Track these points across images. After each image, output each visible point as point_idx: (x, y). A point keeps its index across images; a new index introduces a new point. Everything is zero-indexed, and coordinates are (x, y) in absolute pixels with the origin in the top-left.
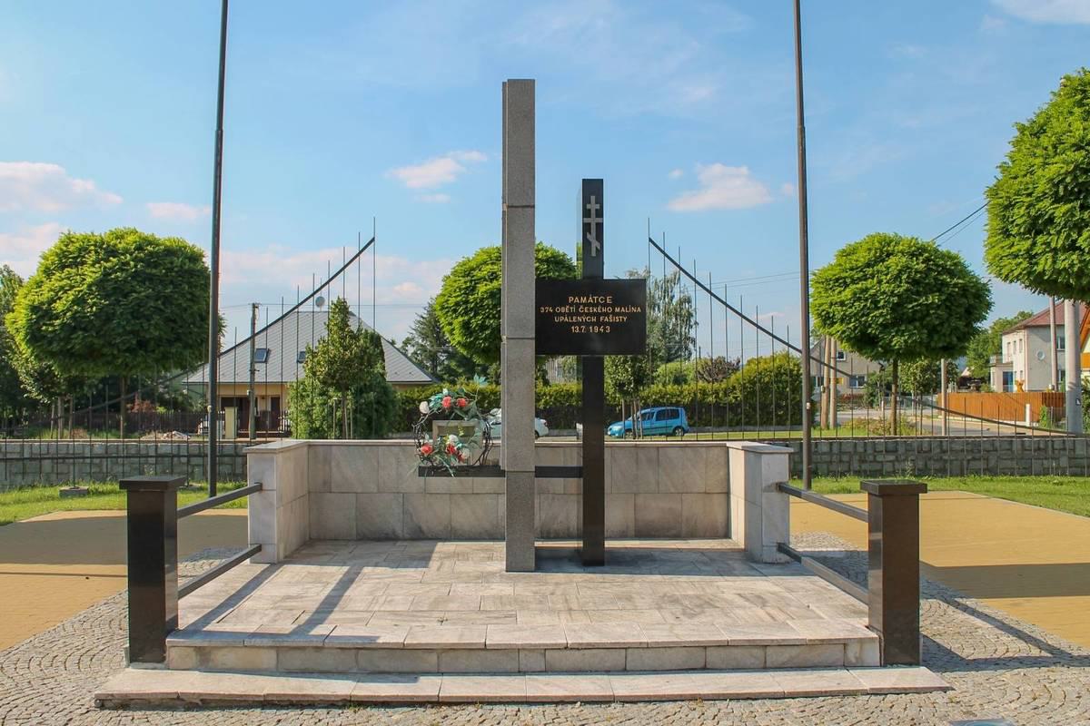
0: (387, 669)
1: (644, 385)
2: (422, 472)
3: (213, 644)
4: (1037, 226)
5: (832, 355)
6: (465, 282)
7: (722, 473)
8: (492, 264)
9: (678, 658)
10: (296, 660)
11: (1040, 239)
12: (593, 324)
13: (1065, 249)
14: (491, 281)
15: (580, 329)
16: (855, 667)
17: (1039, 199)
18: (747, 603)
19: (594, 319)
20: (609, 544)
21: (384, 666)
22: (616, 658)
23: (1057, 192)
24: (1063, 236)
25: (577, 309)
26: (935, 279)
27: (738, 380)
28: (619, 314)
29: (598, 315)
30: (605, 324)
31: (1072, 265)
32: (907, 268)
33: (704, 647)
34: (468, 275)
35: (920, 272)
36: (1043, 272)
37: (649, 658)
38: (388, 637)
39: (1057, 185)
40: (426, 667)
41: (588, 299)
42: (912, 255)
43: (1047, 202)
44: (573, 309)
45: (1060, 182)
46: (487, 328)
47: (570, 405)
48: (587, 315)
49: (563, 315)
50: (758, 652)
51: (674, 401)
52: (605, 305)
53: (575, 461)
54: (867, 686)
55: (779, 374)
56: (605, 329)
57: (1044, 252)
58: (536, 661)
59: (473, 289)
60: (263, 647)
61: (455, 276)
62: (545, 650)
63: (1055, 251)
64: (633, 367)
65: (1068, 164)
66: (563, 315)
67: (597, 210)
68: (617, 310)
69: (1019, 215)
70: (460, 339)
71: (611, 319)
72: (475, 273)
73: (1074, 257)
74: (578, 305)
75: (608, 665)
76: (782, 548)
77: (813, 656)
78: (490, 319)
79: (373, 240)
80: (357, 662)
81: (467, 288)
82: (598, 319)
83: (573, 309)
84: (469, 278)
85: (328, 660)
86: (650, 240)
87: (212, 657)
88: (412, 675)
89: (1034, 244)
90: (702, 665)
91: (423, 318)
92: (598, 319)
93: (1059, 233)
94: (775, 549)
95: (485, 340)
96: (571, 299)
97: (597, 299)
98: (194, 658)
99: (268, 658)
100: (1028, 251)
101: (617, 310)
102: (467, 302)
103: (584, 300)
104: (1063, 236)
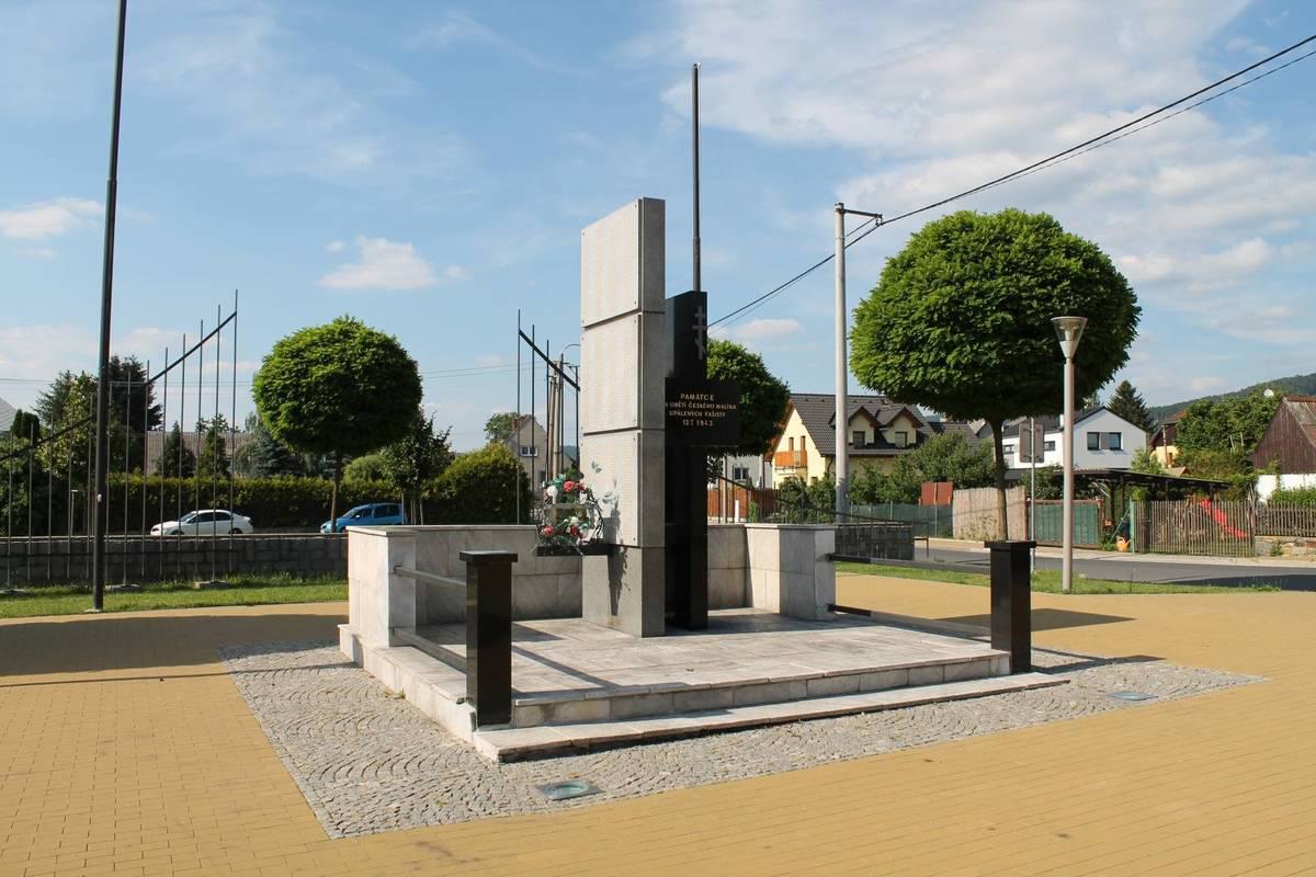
0: (695, 707)
1: (427, 477)
2: (541, 552)
3: (559, 700)
4: (910, 345)
5: (555, 450)
6: (296, 364)
7: (741, 550)
8: (324, 346)
9: (892, 678)
10: (627, 707)
11: (914, 355)
13: (933, 365)
14: (326, 364)
16: (996, 676)
17: (914, 322)
18: (811, 650)
20: (711, 613)
21: (693, 704)
22: (852, 682)
23: (932, 318)
24: (933, 354)
26: (748, 379)
27: (453, 475)
29: (688, 409)
30: (708, 418)
31: (940, 377)
32: (724, 369)
33: (908, 669)
34: (296, 357)
35: (736, 374)
36: (913, 382)
37: (874, 680)
38: (693, 680)
39: (932, 313)
40: (725, 702)
42: (727, 357)
43: (923, 326)
44: (684, 405)
45: (936, 310)
46: (320, 414)
47: (271, 501)
48: (695, 410)
49: (677, 409)
50: (939, 670)
51: (386, 496)
52: (709, 402)
54: (1025, 684)
55: (495, 469)
57: (917, 367)
58: (800, 690)
59: (304, 373)
60: (598, 699)
61: (280, 356)
62: (807, 680)
63: (926, 366)
64: (417, 458)
65: (944, 296)
66: (677, 409)
68: (718, 406)
69: (897, 336)
70: (286, 425)
71: (713, 414)
72: (305, 355)
73: (943, 370)
74: (688, 401)
75: (848, 688)
76: (832, 608)
77: (973, 670)
78: (325, 405)
79: (235, 314)
80: (673, 704)
81: (299, 371)
83: (684, 405)
84: (297, 360)
85: (650, 705)
86: (521, 333)
87: (557, 712)
88: (722, 709)
89: (907, 359)
90: (941, 680)
91: (49, 397)
93: (931, 350)
94: (826, 609)
95: (316, 427)
96: (682, 396)
98: (538, 715)
99: (603, 708)
100: (900, 364)
101: (718, 406)
102: (298, 385)
103: (692, 397)
104: (933, 354)
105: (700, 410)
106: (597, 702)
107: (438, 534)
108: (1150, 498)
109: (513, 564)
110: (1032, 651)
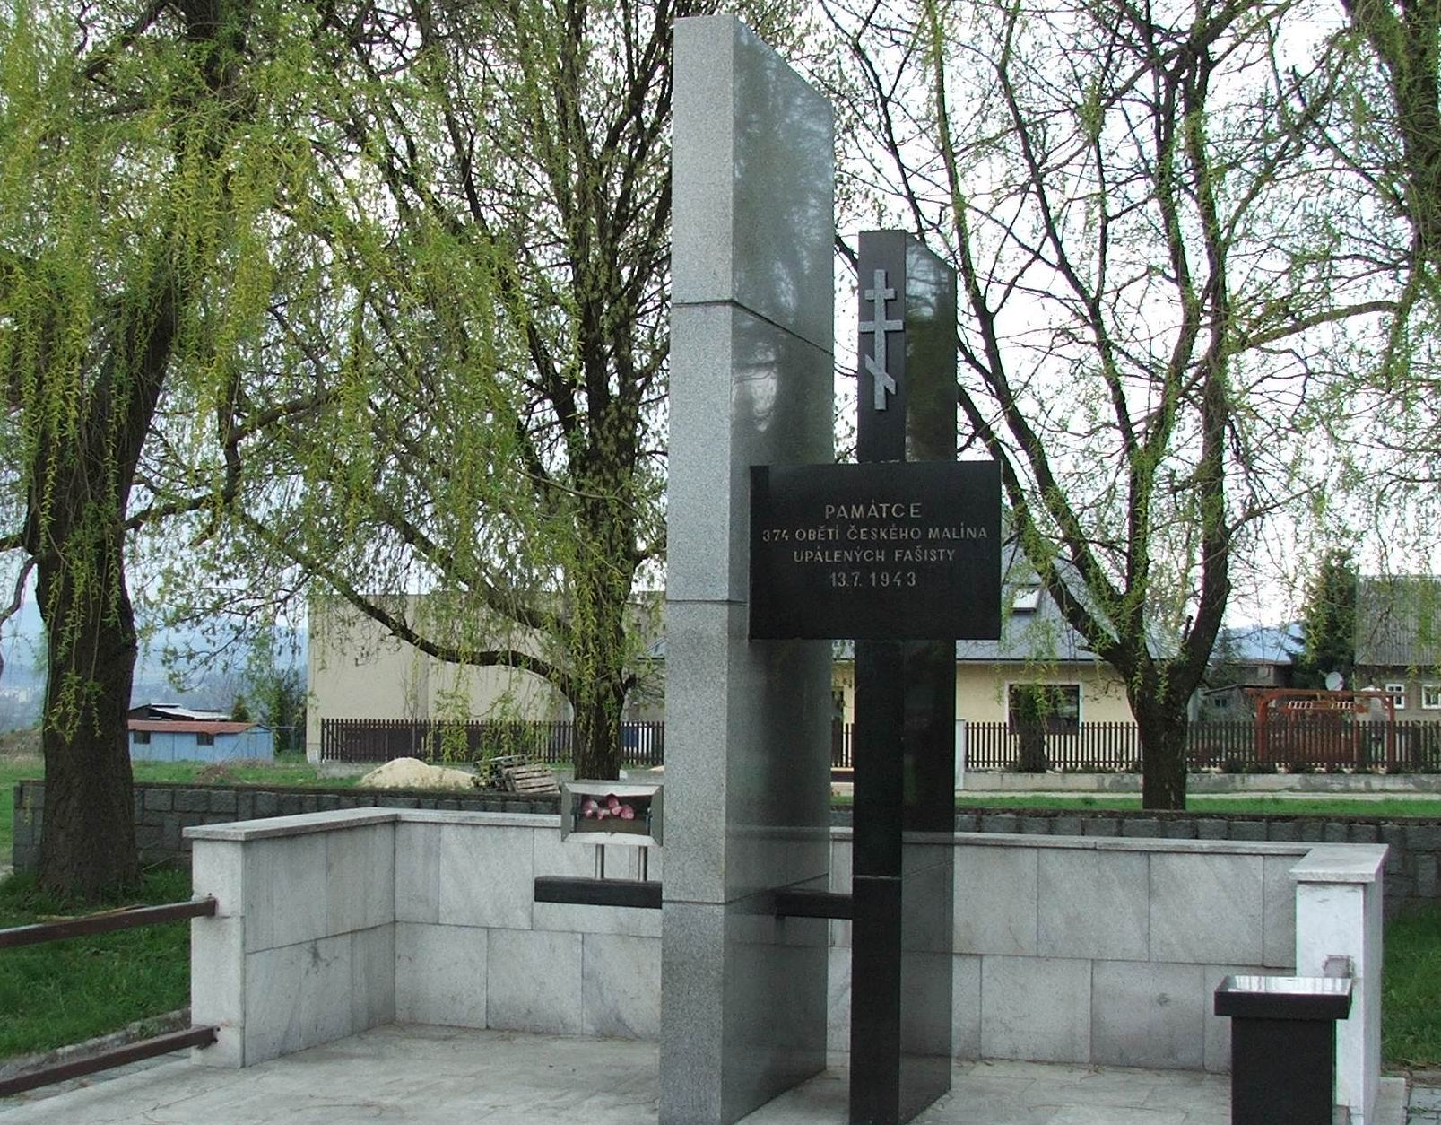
12: (879, 567)
15: (850, 579)
19: (881, 557)
25: (843, 532)
28: (935, 544)
29: (889, 546)
30: (905, 566)
41: (866, 510)
48: (865, 545)
49: (811, 546)
52: (905, 522)
53: (559, 824)
56: (905, 580)
66: (811, 546)
67: (872, 286)
68: (932, 534)
74: (845, 524)
82: (890, 555)
92: (890, 555)
96: (829, 510)
97: (889, 509)
103: (858, 512)
105: (880, 544)
106: (988, 849)
107: (512, 833)
108: (1268, 822)
109: (1340, 1023)
110: (837, 375)
